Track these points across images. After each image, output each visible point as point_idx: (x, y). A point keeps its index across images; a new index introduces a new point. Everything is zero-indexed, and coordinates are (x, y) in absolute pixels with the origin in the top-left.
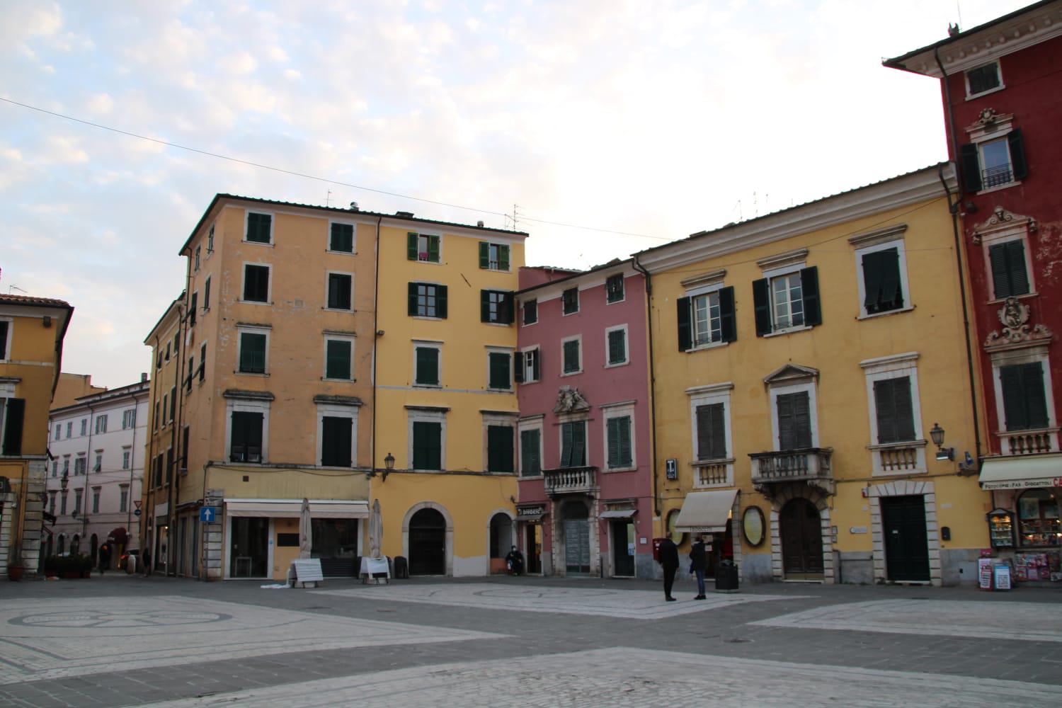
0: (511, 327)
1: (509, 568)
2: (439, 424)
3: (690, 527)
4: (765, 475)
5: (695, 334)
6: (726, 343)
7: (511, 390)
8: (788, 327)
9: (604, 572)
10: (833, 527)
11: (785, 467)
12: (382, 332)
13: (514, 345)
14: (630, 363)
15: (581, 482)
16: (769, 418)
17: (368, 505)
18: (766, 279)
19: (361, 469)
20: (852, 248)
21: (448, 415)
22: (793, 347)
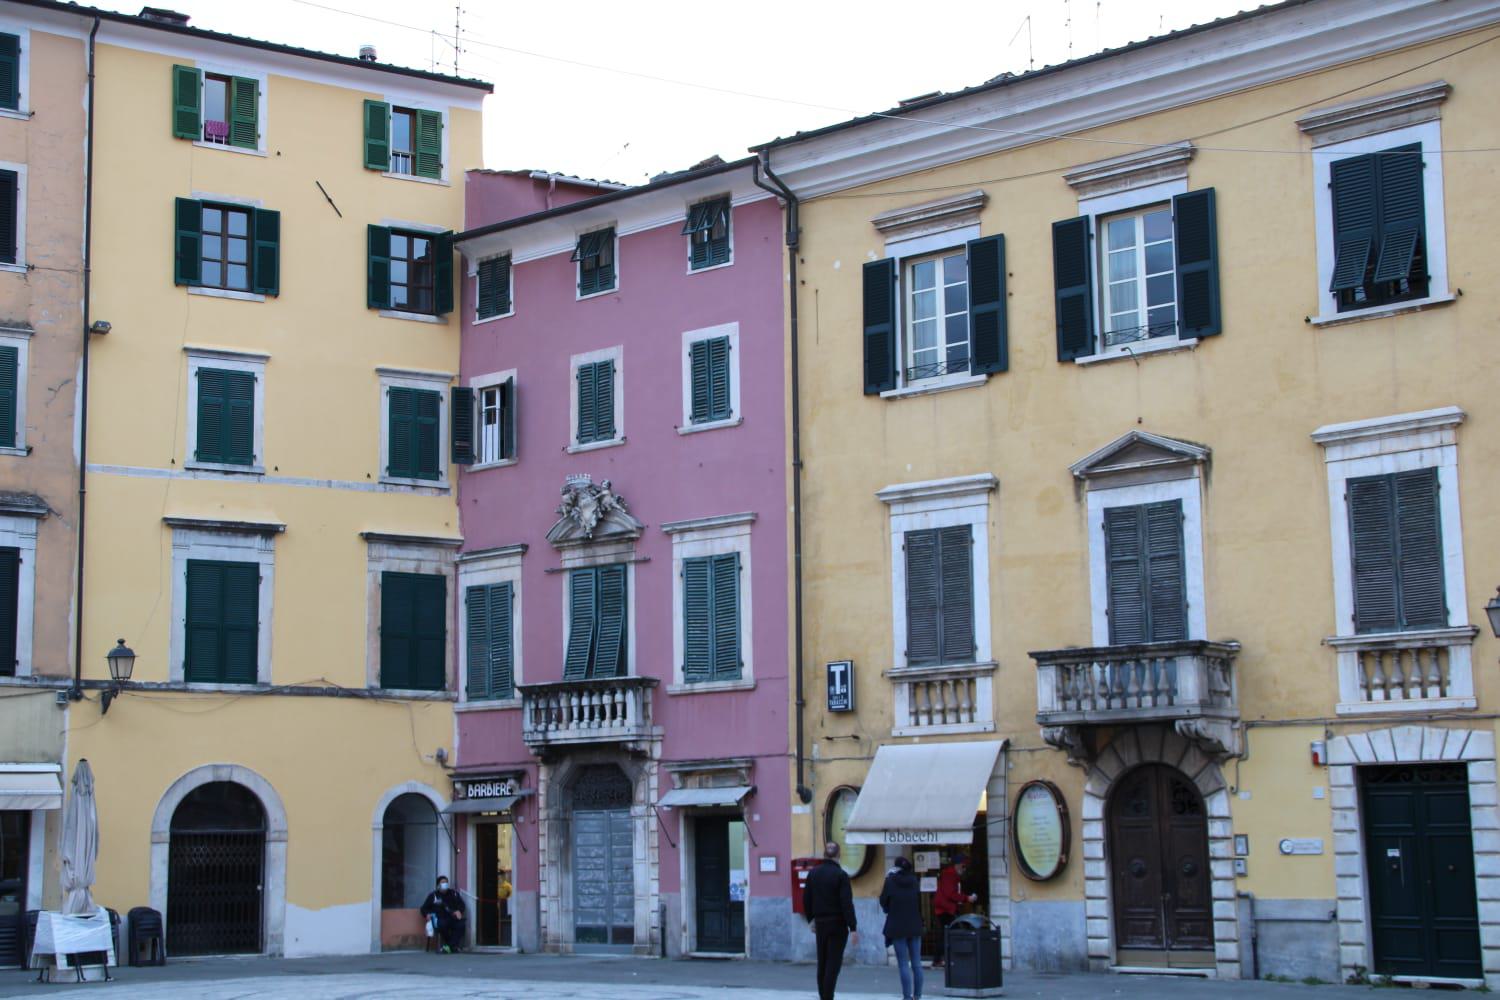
0: (446, 323)
1: (430, 932)
2: (254, 567)
3: (885, 831)
4: (1072, 704)
5: (906, 354)
6: (983, 377)
7: (443, 482)
8: (1137, 339)
9: (669, 943)
10: (1236, 836)
11: (1120, 685)
12: (105, 324)
13: (452, 370)
14: (741, 421)
15: (614, 716)
16: (1084, 566)
17: (59, 774)
18: (1087, 218)
19: (43, 682)
20: (1307, 142)
21: (278, 543)
22: (1149, 388)
